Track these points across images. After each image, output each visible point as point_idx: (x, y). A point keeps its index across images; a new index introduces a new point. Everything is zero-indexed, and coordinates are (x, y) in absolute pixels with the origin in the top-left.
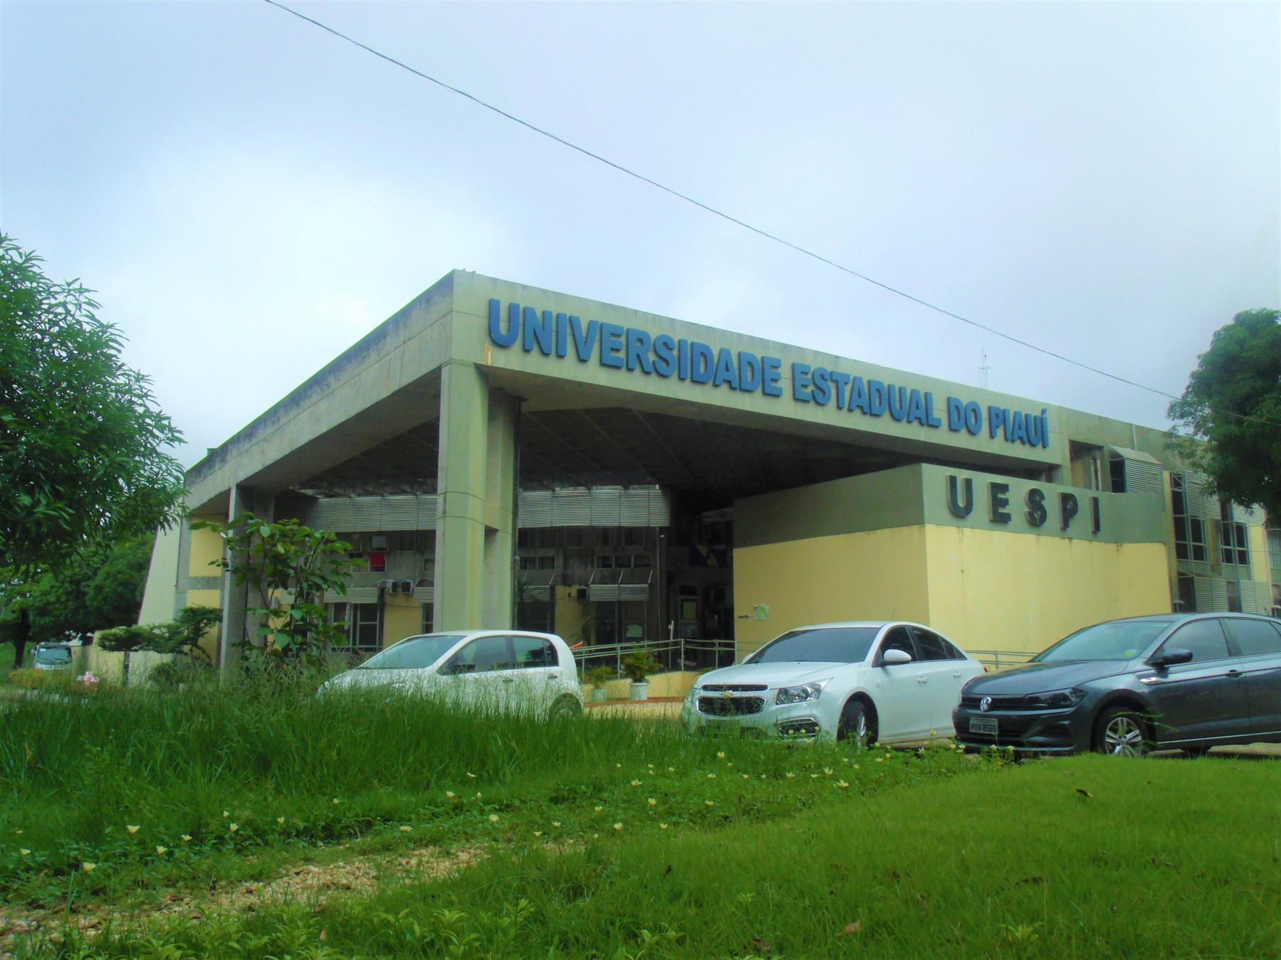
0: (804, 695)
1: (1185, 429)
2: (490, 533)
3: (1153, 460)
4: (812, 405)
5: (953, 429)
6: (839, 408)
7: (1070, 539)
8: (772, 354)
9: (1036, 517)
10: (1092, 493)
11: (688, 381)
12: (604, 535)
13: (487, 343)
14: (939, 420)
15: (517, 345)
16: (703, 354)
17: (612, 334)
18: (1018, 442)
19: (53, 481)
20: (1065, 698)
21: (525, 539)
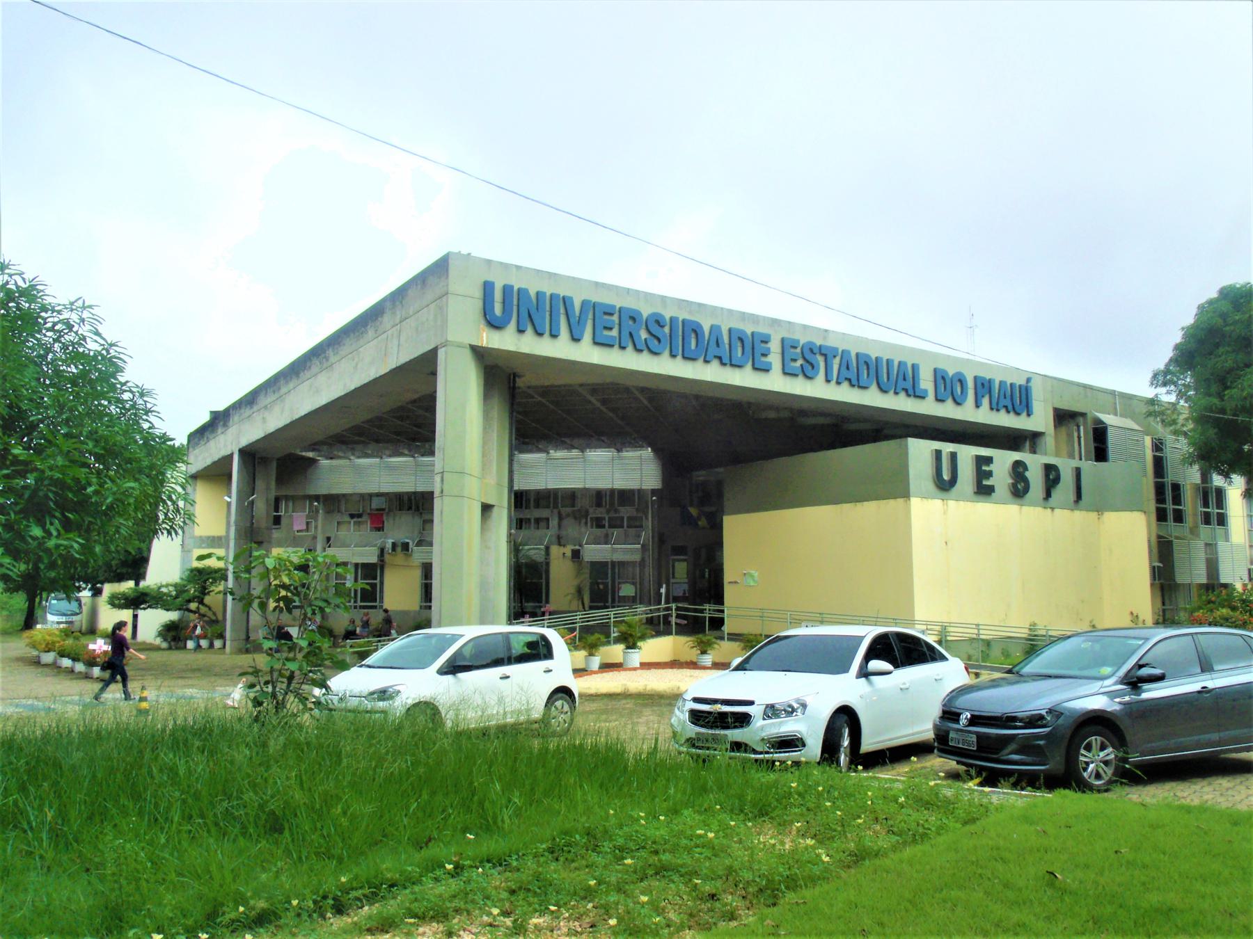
0: (790, 711)
1: (1167, 396)
2: (486, 508)
3: (1136, 427)
4: (801, 378)
5: (939, 400)
6: (828, 381)
7: (1053, 509)
8: (762, 329)
9: (1019, 489)
10: (1075, 463)
11: (679, 357)
12: (599, 496)
13: (483, 325)
14: (926, 391)
15: (512, 326)
16: (695, 331)
17: (605, 313)
18: (1003, 411)
19: (63, 506)
20: (1041, 717)
21: (520, 499)
